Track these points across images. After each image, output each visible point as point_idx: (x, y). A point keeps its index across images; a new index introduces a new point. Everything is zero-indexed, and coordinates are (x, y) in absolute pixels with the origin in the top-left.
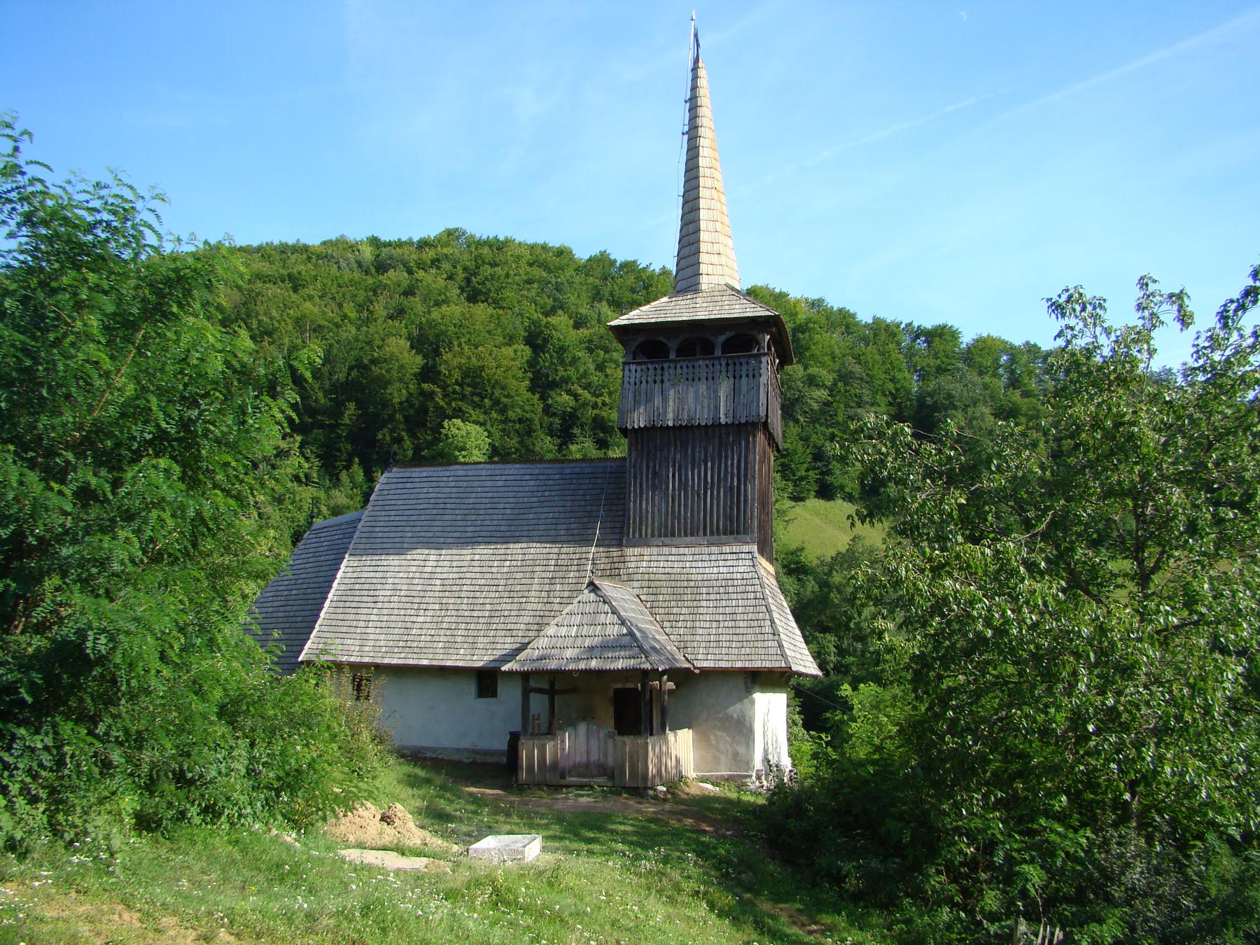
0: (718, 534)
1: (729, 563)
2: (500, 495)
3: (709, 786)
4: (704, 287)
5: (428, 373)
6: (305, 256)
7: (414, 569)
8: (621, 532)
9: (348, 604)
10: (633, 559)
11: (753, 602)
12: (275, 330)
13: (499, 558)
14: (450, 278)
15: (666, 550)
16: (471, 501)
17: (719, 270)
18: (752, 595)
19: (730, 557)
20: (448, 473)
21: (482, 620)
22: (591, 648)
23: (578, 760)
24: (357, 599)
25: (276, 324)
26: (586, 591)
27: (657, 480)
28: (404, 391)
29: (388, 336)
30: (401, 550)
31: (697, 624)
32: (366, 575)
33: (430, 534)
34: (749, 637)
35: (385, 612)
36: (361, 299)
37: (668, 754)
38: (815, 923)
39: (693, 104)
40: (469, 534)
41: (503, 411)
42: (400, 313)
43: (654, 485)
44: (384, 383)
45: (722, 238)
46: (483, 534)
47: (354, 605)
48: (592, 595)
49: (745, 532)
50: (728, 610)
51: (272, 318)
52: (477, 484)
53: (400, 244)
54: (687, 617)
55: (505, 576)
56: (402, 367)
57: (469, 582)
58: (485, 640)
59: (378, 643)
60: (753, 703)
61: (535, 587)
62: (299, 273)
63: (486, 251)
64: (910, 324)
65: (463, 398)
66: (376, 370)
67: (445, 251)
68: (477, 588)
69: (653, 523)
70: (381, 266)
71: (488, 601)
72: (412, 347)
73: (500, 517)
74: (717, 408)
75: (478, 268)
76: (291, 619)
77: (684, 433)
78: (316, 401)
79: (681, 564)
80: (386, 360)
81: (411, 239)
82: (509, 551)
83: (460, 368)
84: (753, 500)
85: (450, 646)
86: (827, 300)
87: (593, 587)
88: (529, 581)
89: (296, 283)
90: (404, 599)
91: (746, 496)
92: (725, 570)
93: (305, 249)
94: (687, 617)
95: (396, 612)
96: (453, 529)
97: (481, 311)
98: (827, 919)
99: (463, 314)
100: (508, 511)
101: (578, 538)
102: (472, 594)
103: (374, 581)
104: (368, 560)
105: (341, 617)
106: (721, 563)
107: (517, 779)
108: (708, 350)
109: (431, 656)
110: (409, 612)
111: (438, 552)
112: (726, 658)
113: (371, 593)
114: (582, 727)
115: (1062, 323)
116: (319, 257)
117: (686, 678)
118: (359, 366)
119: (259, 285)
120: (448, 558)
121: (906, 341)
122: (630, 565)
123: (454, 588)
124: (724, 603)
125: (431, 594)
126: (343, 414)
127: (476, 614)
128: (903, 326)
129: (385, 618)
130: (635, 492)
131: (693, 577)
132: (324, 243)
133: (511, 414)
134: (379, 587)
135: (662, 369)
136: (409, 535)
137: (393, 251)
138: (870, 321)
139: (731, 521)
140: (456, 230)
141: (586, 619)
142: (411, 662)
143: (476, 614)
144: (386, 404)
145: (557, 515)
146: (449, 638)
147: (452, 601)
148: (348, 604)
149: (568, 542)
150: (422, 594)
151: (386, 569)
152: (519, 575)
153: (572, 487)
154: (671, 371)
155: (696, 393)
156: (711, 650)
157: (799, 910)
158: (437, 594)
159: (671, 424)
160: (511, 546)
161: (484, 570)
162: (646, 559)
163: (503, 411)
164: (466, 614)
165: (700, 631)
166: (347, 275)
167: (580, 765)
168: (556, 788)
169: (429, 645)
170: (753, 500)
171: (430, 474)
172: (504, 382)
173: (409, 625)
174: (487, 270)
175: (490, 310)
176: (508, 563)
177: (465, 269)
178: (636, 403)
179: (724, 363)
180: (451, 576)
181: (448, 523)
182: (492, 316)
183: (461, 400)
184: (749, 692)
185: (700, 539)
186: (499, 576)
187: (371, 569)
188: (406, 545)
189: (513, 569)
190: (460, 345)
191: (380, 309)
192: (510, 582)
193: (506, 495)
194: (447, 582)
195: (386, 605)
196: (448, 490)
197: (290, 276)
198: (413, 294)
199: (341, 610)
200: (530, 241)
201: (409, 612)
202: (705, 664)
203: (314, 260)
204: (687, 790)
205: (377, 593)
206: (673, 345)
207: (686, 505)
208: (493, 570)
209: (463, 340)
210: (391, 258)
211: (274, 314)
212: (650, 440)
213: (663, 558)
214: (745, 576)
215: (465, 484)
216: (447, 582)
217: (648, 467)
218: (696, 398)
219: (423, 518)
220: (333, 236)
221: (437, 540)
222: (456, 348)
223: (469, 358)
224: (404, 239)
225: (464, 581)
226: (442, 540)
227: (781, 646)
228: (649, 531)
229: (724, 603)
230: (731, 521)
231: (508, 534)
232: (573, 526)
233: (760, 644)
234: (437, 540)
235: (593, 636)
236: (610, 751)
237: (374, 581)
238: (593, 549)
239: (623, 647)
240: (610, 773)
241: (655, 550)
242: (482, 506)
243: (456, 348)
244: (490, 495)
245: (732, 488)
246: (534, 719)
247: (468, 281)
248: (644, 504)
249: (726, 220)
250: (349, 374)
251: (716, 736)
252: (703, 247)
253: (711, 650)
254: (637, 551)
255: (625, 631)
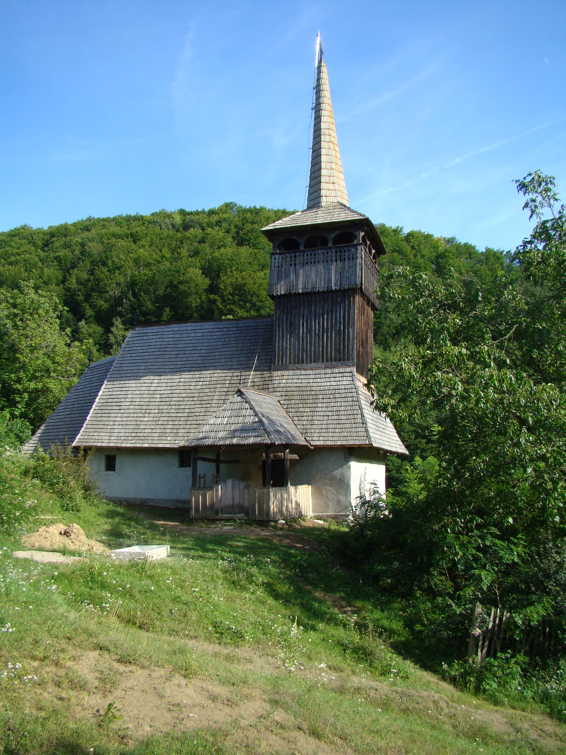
0: (331, 361)
1: (337, 379)
2: (199, 341)
3: (321, 522)
4: (323, 204)
5: (213, 289)
6: (141, 222)
7: (144, 389)
8: (270, 361)
9: (104, 411)
10: (277, 378)
11: (351, 403)
12: (122, 266)
13: (195, 380)
14: (228, 232)
15: (298, 372)
16: (181, 346)
17: (333, 193)
18: (351, 399)
19: (338, 375)
20: (169, 330)
21: (182, 419)
22: (235, 431)
23: (227, 503)
24: (109, 408)
25: (123, 263)
26: (236, 396)
27: (293, 329)
28: (198, 300)
29: (188, 267)
30: (137, 376)
31: (315, 418)
32: (116, 393)
33: (156, 367)
34: (347, 426)
35: (125, 415)
36: (173, 246)
37: (289, 500)
38: (350, 606)
39: (318, 89)
40: (178, 366)
41: (258, 310)
42: (196, 253)
43: (290, 331)
44: (186, 295)
45: (335, 173)
46: (187, 366)
47: (107, 411)
48: (239, 398)
49: (348, 359)
50: (335, 409)
51: (120, 259)
52: (185, 335)
53: (197, 213)
54: (309, 414)
55: (199, 391)
56: (197, 285)
57: (176, 395)
58: (184, 431)
59: (120, 435)
60: (349, 468)
61: (216, 398)
62: (137, 232)
63: (248, 215)
64: (509, 252)
65: (234, 303)
66: (182, 287)
67: (224, 216)
68: (181, 399)
69: (290, 355)
70: (186, 227)
71: (187, 407)
72: (203, 273)
73: (198, 355)
74: (330, 280)
75: (243, 225)
76: (73, 422)
77: (310, 297)
78: (147, 308)
79: (307, 381)
80: (187, 282)
81: (204, 210)
82: (202, 376)
83: (232, 285)
84: (353, 338)
85: (162, 435)
86: (457, 238)
87: (240, 393)
88: (212, 394)
89: (135, 238)
90: (137, 407)
91: (348, 336)
92: (334, 383)
93: (142, 218)
94: (309, 414)
95: (132, 415)
96: (169, 363)
97: (245, 251)
98: (359, 604)
99: (233, 253)
100: (203, 351)
101: (244, 366)
102: (178, 403)
103: (120, 396)
104: (117, 384)
105: (99, 419)
106: (332, 379)
107: (189, 515)
108: (324, 243)
109: (150, 442)
110: (139, 415)
111: (159, 378)
112: (331, 439)
113: (118, 404)
114: (230, 482)
115: (528, 197)
116: (149, 222)
117: (307, 453)
118: (171, 285)
119: (114, 240)
120: (165, 381)
121: (507, 261)
122: (275, 382)
123: (167, 400)
124: (332, 404)
125: (153, 403)
126: (162, 314)
127: (179, 415)
128: (504, 253)
129: (125, 419)
130: (279, 335)
131: (314, 389)
132: (153, 214)
133: (263, 312)
134: (123, 400)
135: (295, 256)
136: (143, 368)
137: (193, 217)
138: (484, 251)
139: (340, 353)
140: (231, 203)
141: (234, 413)
142: (138, 445)
143: (179, 415)
144: (188, 307)
145: (232, 352)
146: (163, 431)
147: (166, 407)
148: (104, 411)
149: (238, 369)
150: (148, 404)
151: (127, 389)
152: (207, 391)
153: (243, 335)
154: (301, 258)
155: (317, 271)
156: (322, 434)
157: (342, 598)
158: (157, 403)
159: (300, 291)
160: (204, 372)
161: (186, 388)
162: (285, 378)
163: (258, 310)
164: (174, 415)
165: (316, 422)
166: (165, 232)
167: (228, 506)
168: (213, 521)
169: (149, 435)
170: (353, 338)
171: (158, 330)
172: (258, 292)
173: (139, 423)
174: (249, 227)
175: (250, 250)
176: (201, 383)
177: (236, 226)
178: (279, 279)
179: (334, 251)
180: (166, 392)
181: (166, 360)
182: (251, 253)
183: (232, 304)
184: (347, 461)
185: (320, 365)
186: (195, 391)
187: (119, 389)
188: (140, 374)
189: (203, 387)
190: (231, 272)
191: (184, 252)
192: (201, 395)
193: (203, 341)
194: (163, 396)
195: (126, 411)
196: (168, 340)
197: (131, 234)
198: (205, 242)
199: (99, 415)
200: (275, 208)
201: (139, 415)
202: (317, 443)
203: (146, 224)
204: (303, 523)
205: (121, 404)
206: (302, 241)
207: (311, 343)
208: (192, 388)
209: (233, 268)
210: (192, 221)
211: (122, 256)
212: (289, 303)
213: (296, 377)
214: (347, 387)
215: (178, 336)
216: (163, 396)
217: (287, 319)
218: (316, 275)
219: (152, 357)
220: (157, 210)
221: (159, 370)
222: (229, 273)
223: (237, 278)
224: (199, 210)
225: (173, 395)
226: (162, 370)
227: (367, 431)
228: (288, 360)
229: (332, 404)
230: (340, 353)
231: (202, 365)
232: (242, 359)
233: (353, 430)
234: (159, 370)
235: (237, 423)
236: (246, 497)
237: (120, 396)
238: (252, 373)
239: (254, 430)
240: (245, 510)
241: (291, 372)
242: (188, 349)
243: (229, 273)
244: (193, 342)
245: (340, 331)
246: (200, 478)
247: (238, 233)
248: (285, 343)
249: (339, 162)
250: (165, 291)
251: (326, 490)
252: (323, 179)
253: (322, 434)
254: (280, 373)
255: (257, 420)
